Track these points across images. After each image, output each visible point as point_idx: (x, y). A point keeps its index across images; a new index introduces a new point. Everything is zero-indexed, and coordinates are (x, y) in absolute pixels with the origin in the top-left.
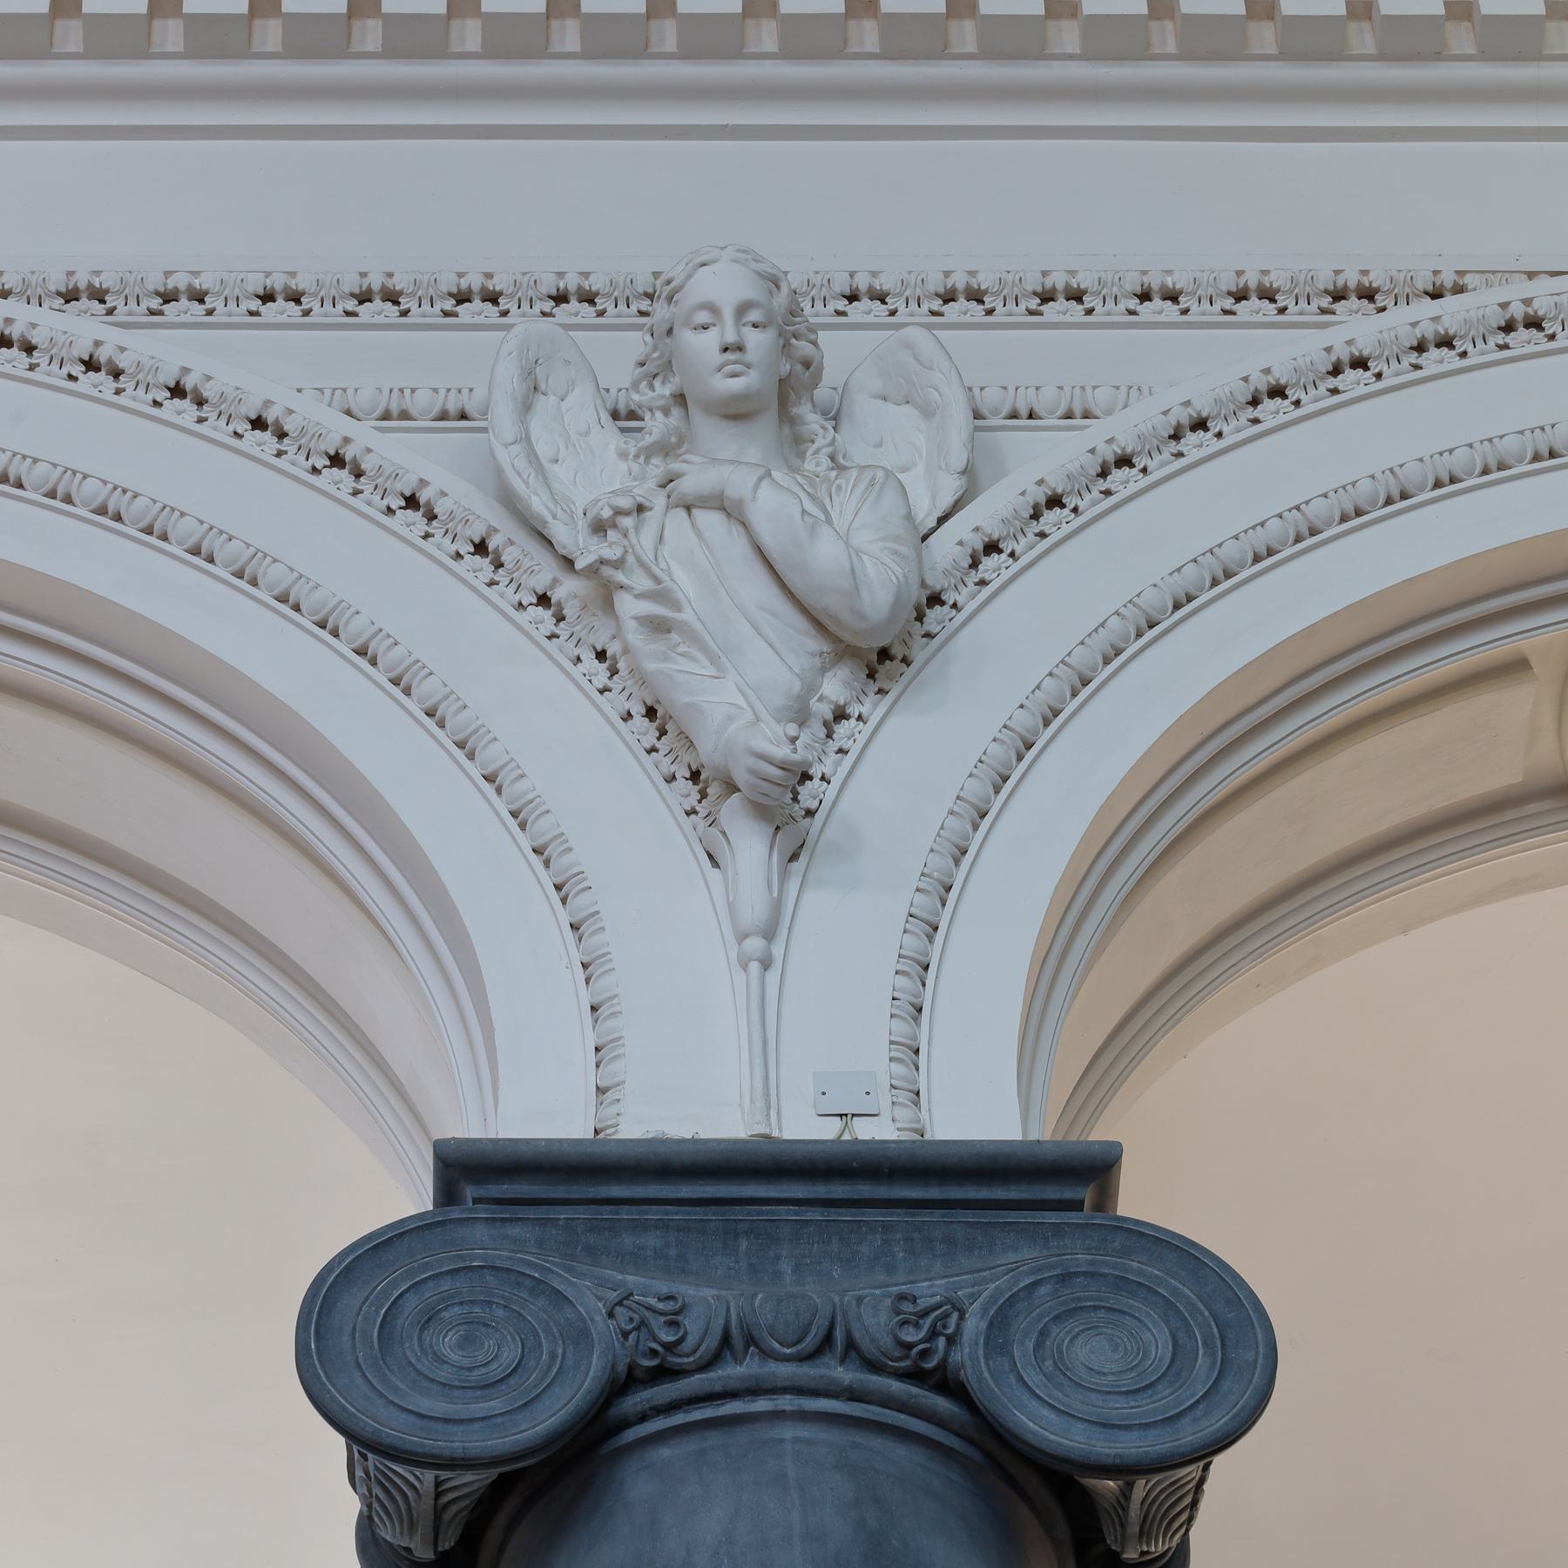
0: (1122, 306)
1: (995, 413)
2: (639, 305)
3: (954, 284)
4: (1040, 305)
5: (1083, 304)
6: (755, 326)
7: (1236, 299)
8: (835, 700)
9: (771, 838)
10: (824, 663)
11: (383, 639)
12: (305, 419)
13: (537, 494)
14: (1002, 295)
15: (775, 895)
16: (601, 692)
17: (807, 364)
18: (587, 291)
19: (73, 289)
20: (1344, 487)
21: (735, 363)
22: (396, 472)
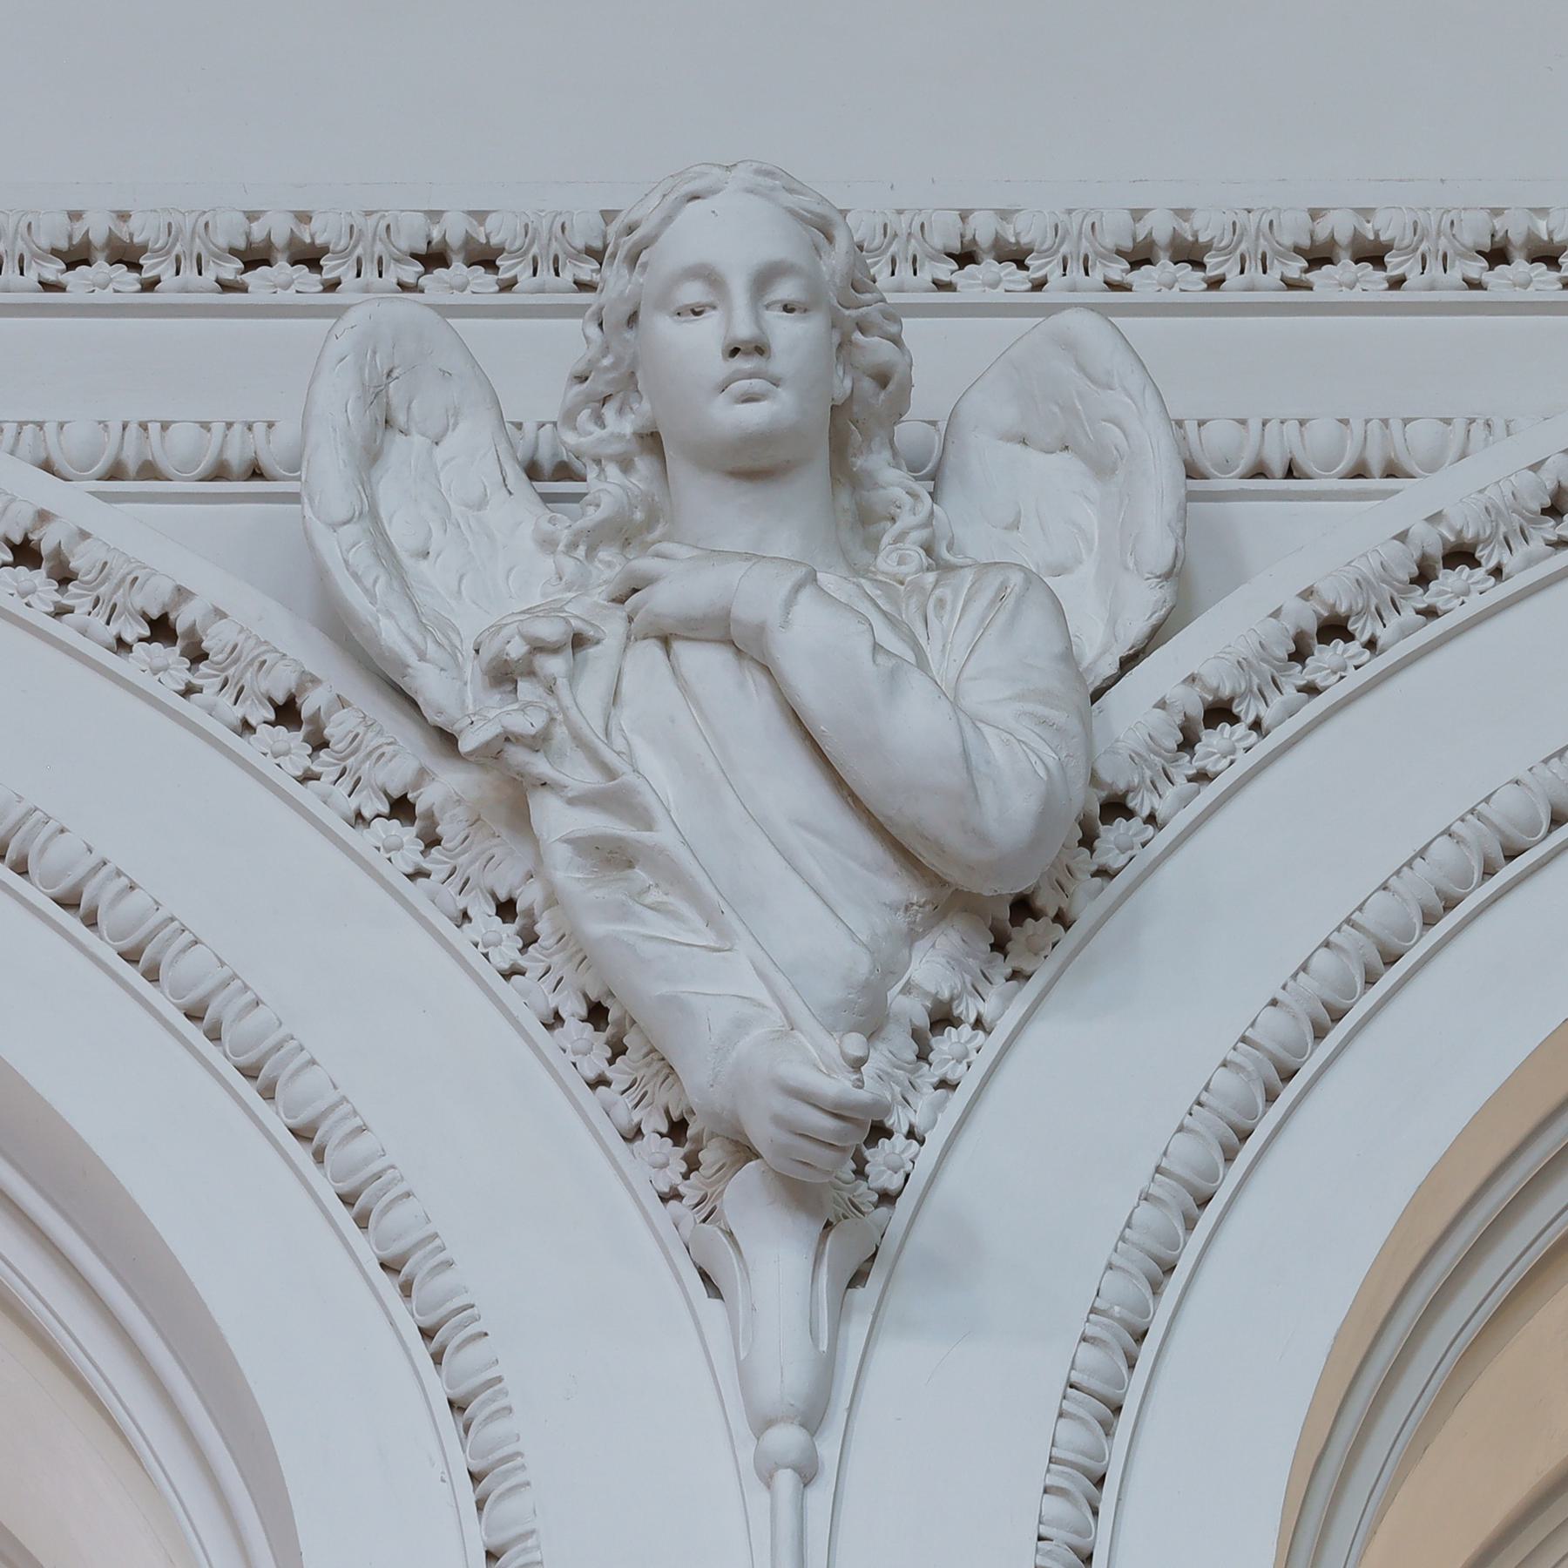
0: (926, 276)
1: (1226, 467)
5: (321, 273)
6: (788, 308)
8: (933, 991)
9: (814, 1245)
11: (108, 879)
15: (824, 1347)
16: (507, 975)
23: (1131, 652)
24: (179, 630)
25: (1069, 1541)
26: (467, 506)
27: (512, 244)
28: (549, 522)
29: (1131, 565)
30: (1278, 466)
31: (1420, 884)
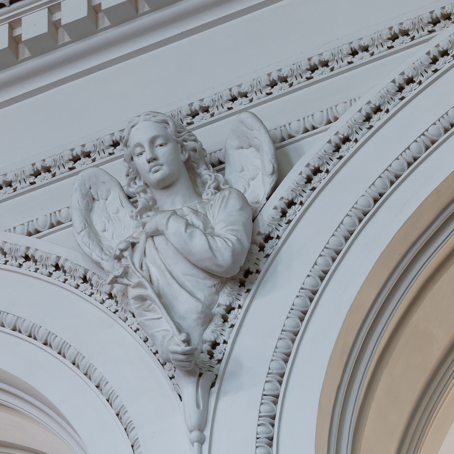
1: (298, 133)
4: (312, 73)
6: (161, 145)
7: (192, 117)
8: (225, 304)
9: (196, 383)
10: (218, 288)
11: (51, 336)
12: (10, 244)
13: (94, 252)
14: (294, 75)
16: (5, 264)
17: (195, 150)
18: (363, 46)
20: (442, 117)
21: (154, 166)
23: (268, 196)
25: (266, 437)
26: (114, 214)
28: (131, 212)
29: (265, 174)
31: (343, 231)
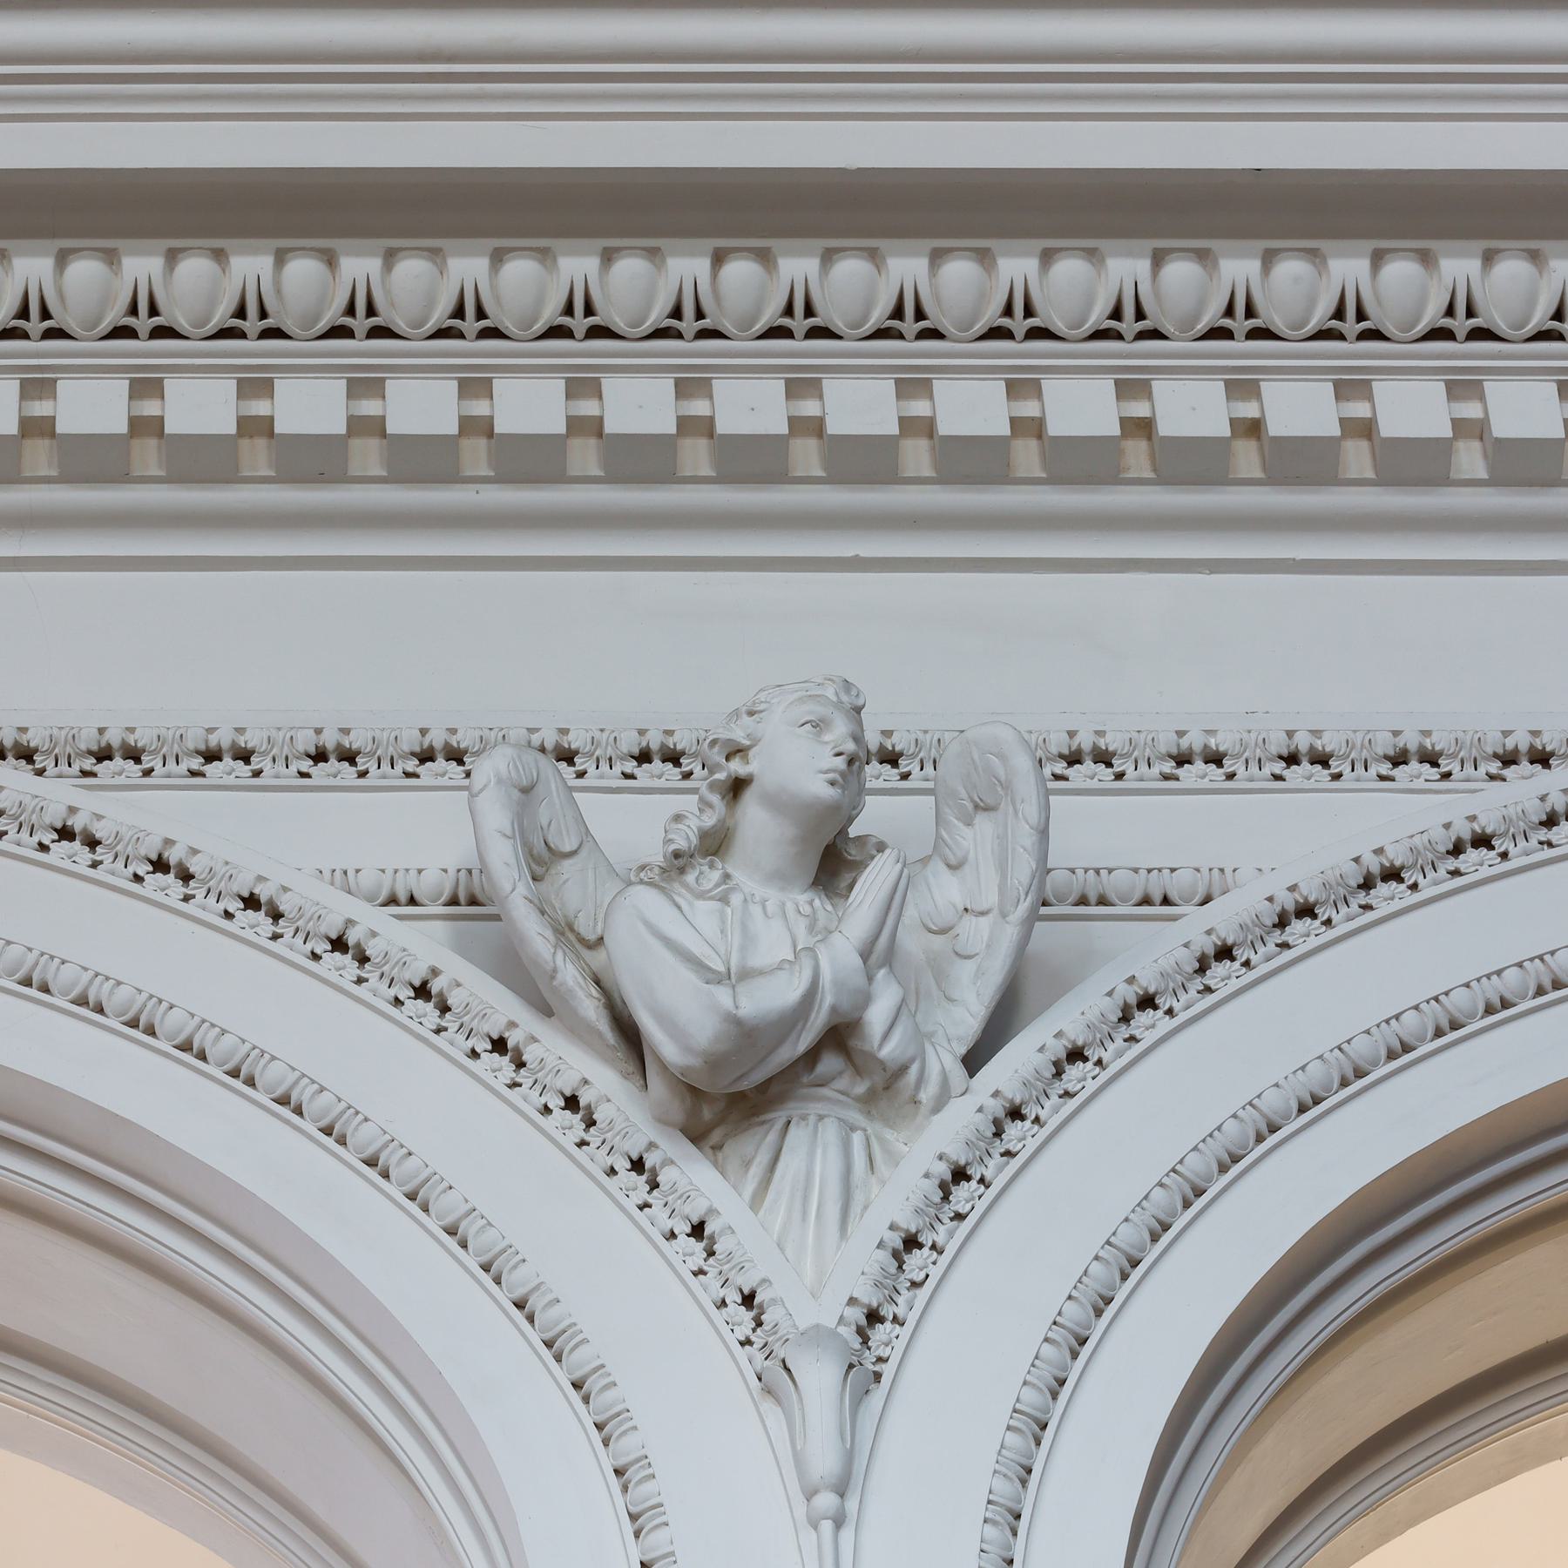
2: (189, 762)
3: (1080, 744)
7: (1068, 763)
8: (905, 1227)
15: (848, 1446)
16: (641, 1208)
18: (241, 747)
19: (1076, 750)
22: (404, 960)
24: (433, 993)
27: (690, 750)
30: (403, 897)
